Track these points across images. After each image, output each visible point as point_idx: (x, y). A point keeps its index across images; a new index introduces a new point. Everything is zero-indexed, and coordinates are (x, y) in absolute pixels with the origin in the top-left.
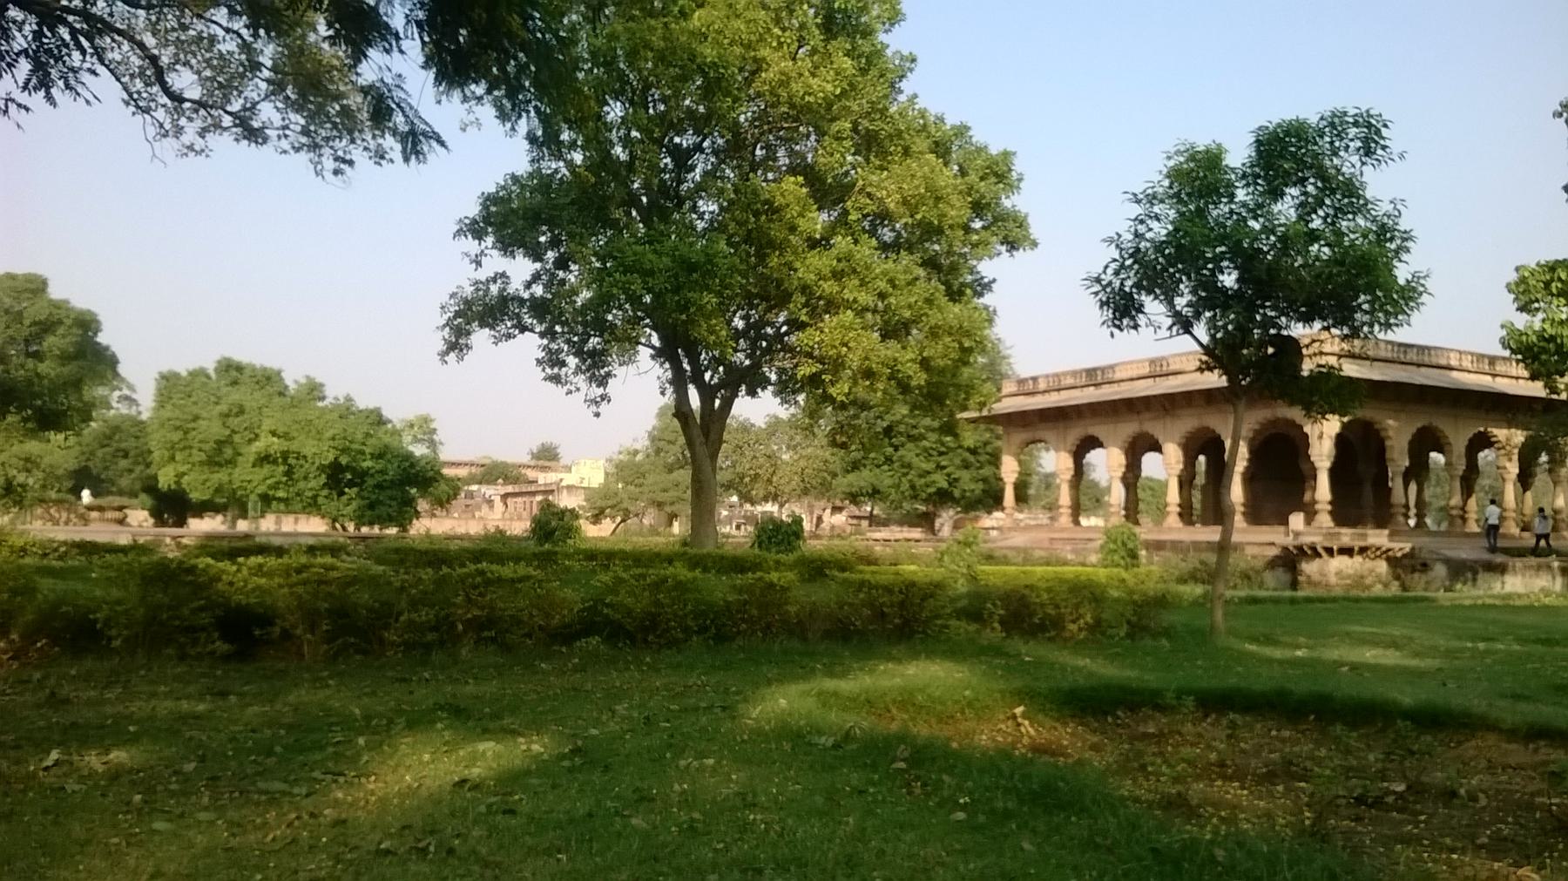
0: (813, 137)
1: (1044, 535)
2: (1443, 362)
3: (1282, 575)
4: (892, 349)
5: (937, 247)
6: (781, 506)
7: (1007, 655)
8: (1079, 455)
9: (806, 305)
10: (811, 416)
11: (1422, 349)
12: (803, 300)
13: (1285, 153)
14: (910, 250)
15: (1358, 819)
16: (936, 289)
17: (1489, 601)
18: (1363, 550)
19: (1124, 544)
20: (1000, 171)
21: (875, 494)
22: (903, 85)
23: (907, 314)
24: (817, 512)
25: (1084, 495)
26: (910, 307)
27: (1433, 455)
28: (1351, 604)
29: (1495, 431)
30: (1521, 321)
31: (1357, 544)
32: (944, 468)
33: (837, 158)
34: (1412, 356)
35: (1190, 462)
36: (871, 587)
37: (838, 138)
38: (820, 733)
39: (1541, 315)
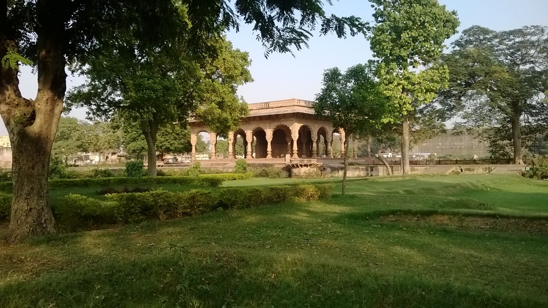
18: (310, 165)
19: (242, 166)
31: (309, 163)
38: (305, 224)
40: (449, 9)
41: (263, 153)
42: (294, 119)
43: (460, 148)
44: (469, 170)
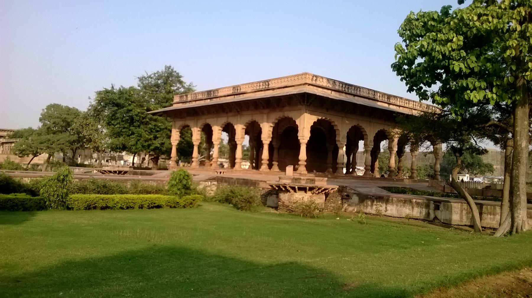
18: (311, 189)
41: (257, 164)
42: (303, 108)
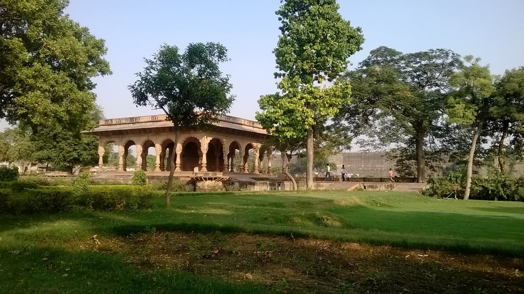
0: (27, 25)
1: (113, 174)
2: (240, 122)
3: (191, 187)
4: (54, 107)
5: (74, 70)
6: (10, 163)
7: (94, 217)
8: (127, 147)
9: (21, 87)
10: (22, 129)
11: (234, 118)
12: (20, 85)
13: (196, 54)
14: (64, 70)
15: (203, 263)
16: (73, 85)
17: (249, 194)
18: (215, 178)
20: (99, 46)
21: (49, 159)
22: (64, 10)
23: (62, 94)
24: (25, 166)
25: (128, 160)
26: (63, 91)
27: (236, 150)
28: (211, 195)
29: (253, 144)
30: (261, 112)
31: (214, 177)
32: (77, 150)
33: (33, 32)
34: (231, 120)
35: (164, 150)
36: (42, 194)
37: (37, 26)
39: (266, 110)
40: (354, 25)
43: (381, 170)
44: (372, 187)
